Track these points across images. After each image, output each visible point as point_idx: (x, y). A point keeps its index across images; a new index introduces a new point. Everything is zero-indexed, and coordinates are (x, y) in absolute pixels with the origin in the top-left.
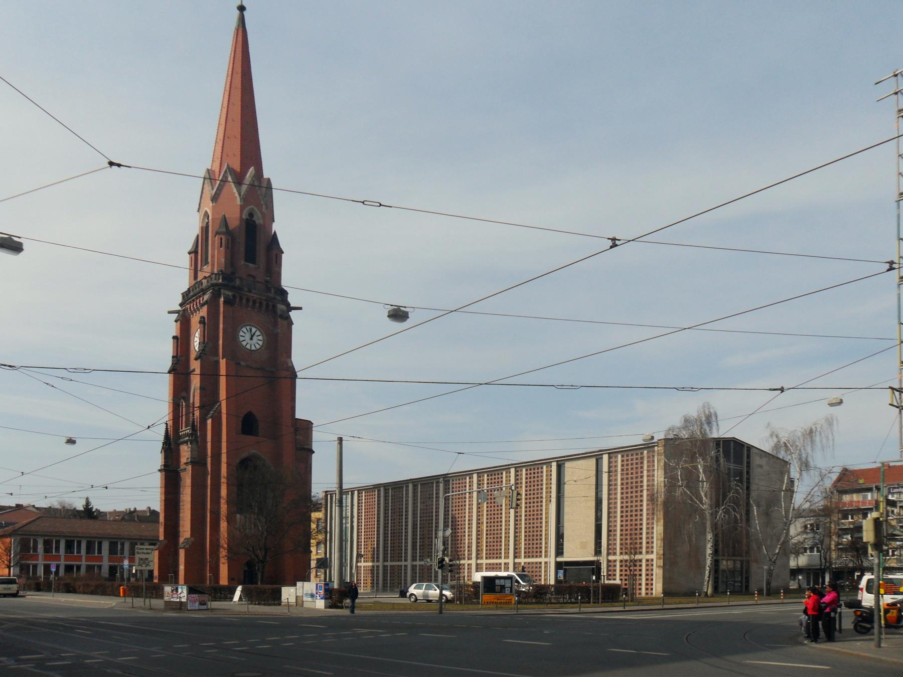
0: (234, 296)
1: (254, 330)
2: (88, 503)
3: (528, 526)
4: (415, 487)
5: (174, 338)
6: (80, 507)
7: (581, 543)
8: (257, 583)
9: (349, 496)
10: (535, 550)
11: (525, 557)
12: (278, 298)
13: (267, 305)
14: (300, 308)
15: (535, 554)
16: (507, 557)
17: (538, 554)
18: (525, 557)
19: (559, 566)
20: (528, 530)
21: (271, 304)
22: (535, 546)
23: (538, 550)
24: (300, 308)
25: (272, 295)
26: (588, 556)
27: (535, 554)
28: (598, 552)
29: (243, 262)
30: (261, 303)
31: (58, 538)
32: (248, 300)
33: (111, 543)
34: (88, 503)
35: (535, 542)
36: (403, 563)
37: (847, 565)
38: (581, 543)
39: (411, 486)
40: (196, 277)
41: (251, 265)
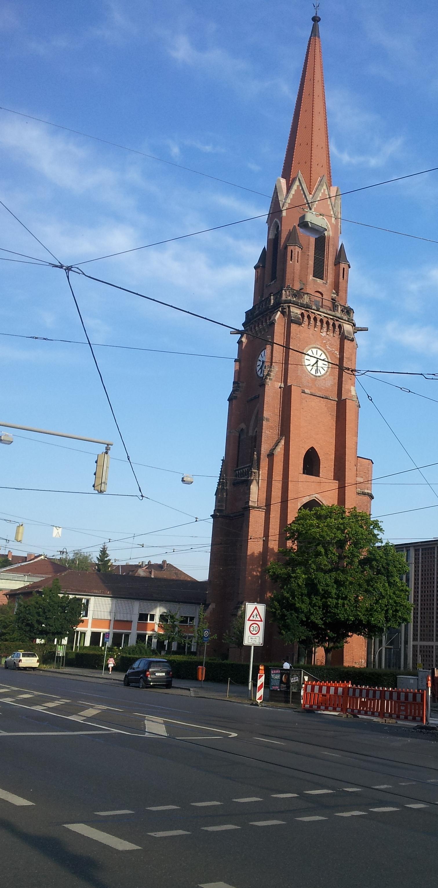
0: (302, 314)
1: (313, 372)
2: (104, 552)
6: (95, 557)
11: (421, 640)
12: (345, 317)
13: (334, 325)
14: (366, 329)
18: (421, 640)
21: (337, 323)
24: (366, 329)
25: (339, 314)
26: (195, 650)
29: (311, 277)
30: (328, 323)
31: (309, 666)
32: (315, 319)
33: (416, 701)
34: (104, 552)
36: (419, 643)
40: (262, 296)
41: (319, 280)
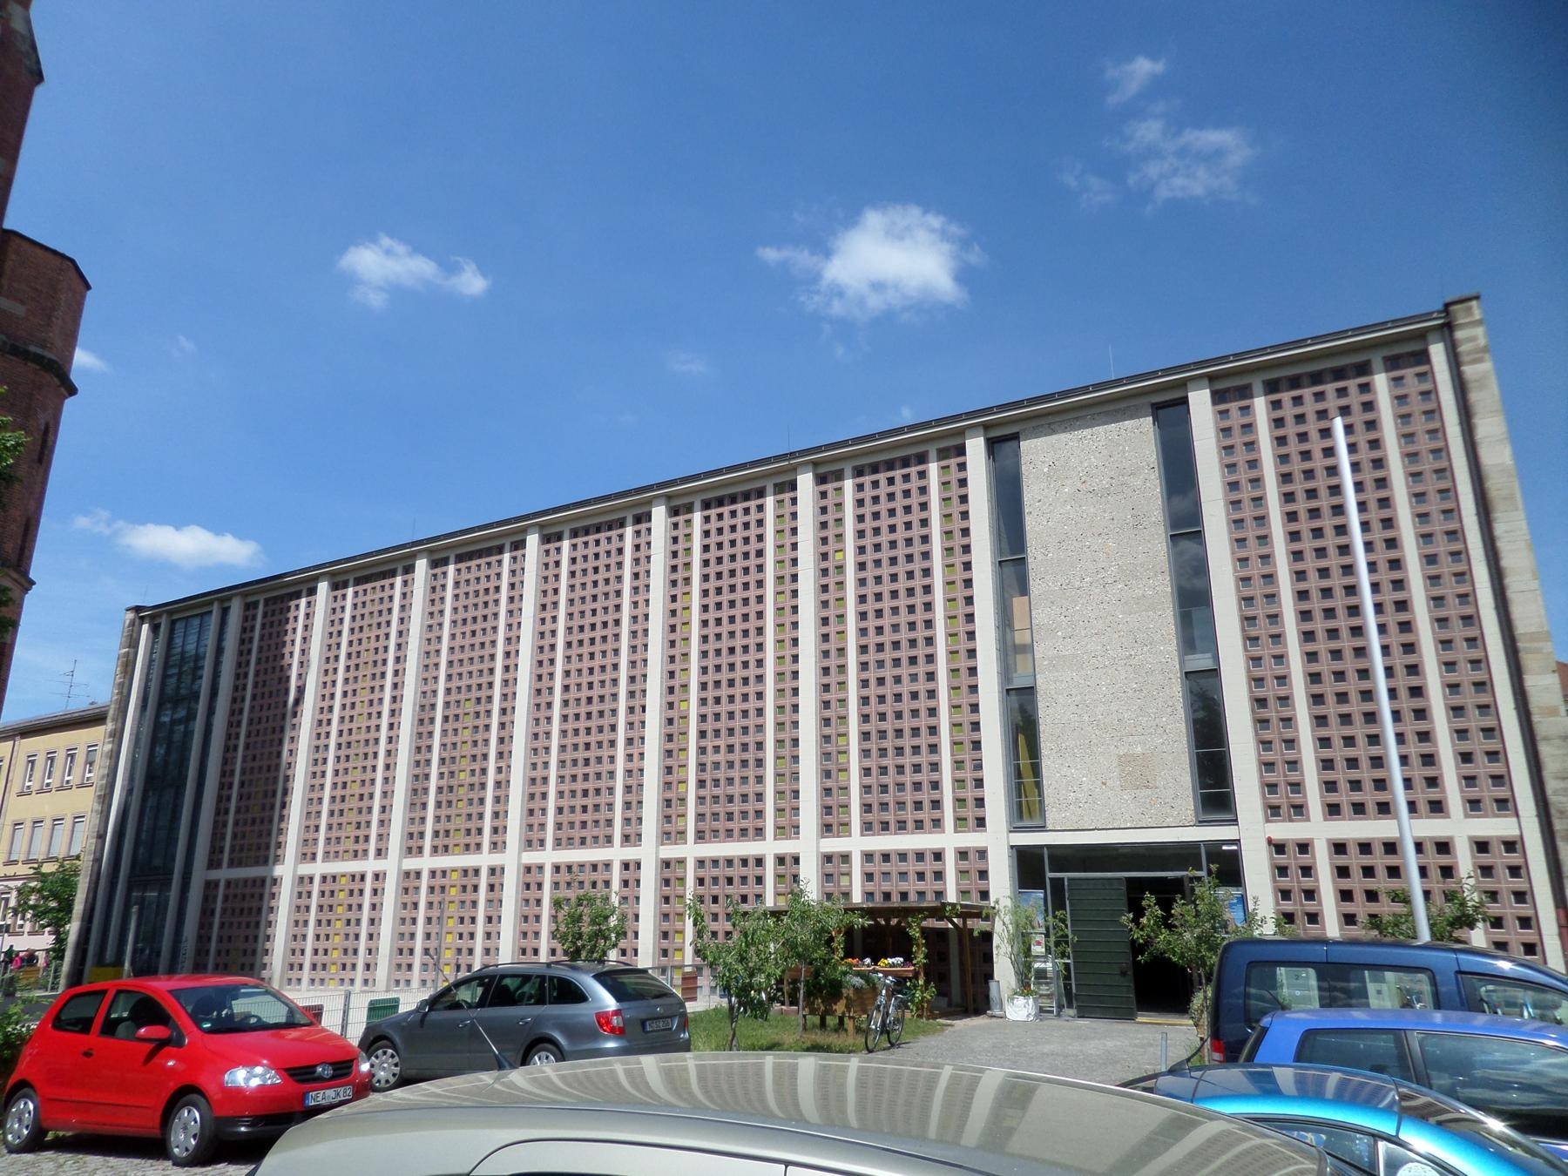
3: (710, 709)
4: (250, 607)
5: (72, 391)
7: (1125, 760)
8: (1051, 871)
9: (194, 631)
10: (909, 797)
11: (867, 827)
15: (910, 815)
16: (789, 829)
17: (926, 815)
18: (867, 827)
19: (1029, 866)
20: (873, 708)
22: (908, 778)
23: (925, 796)
26: (1174, 821)
27: (910, 815)
28: (1215, 792)
35: (908, 760)
37: (713, 989)
38: (1125, 760)
39: (236, 608)
